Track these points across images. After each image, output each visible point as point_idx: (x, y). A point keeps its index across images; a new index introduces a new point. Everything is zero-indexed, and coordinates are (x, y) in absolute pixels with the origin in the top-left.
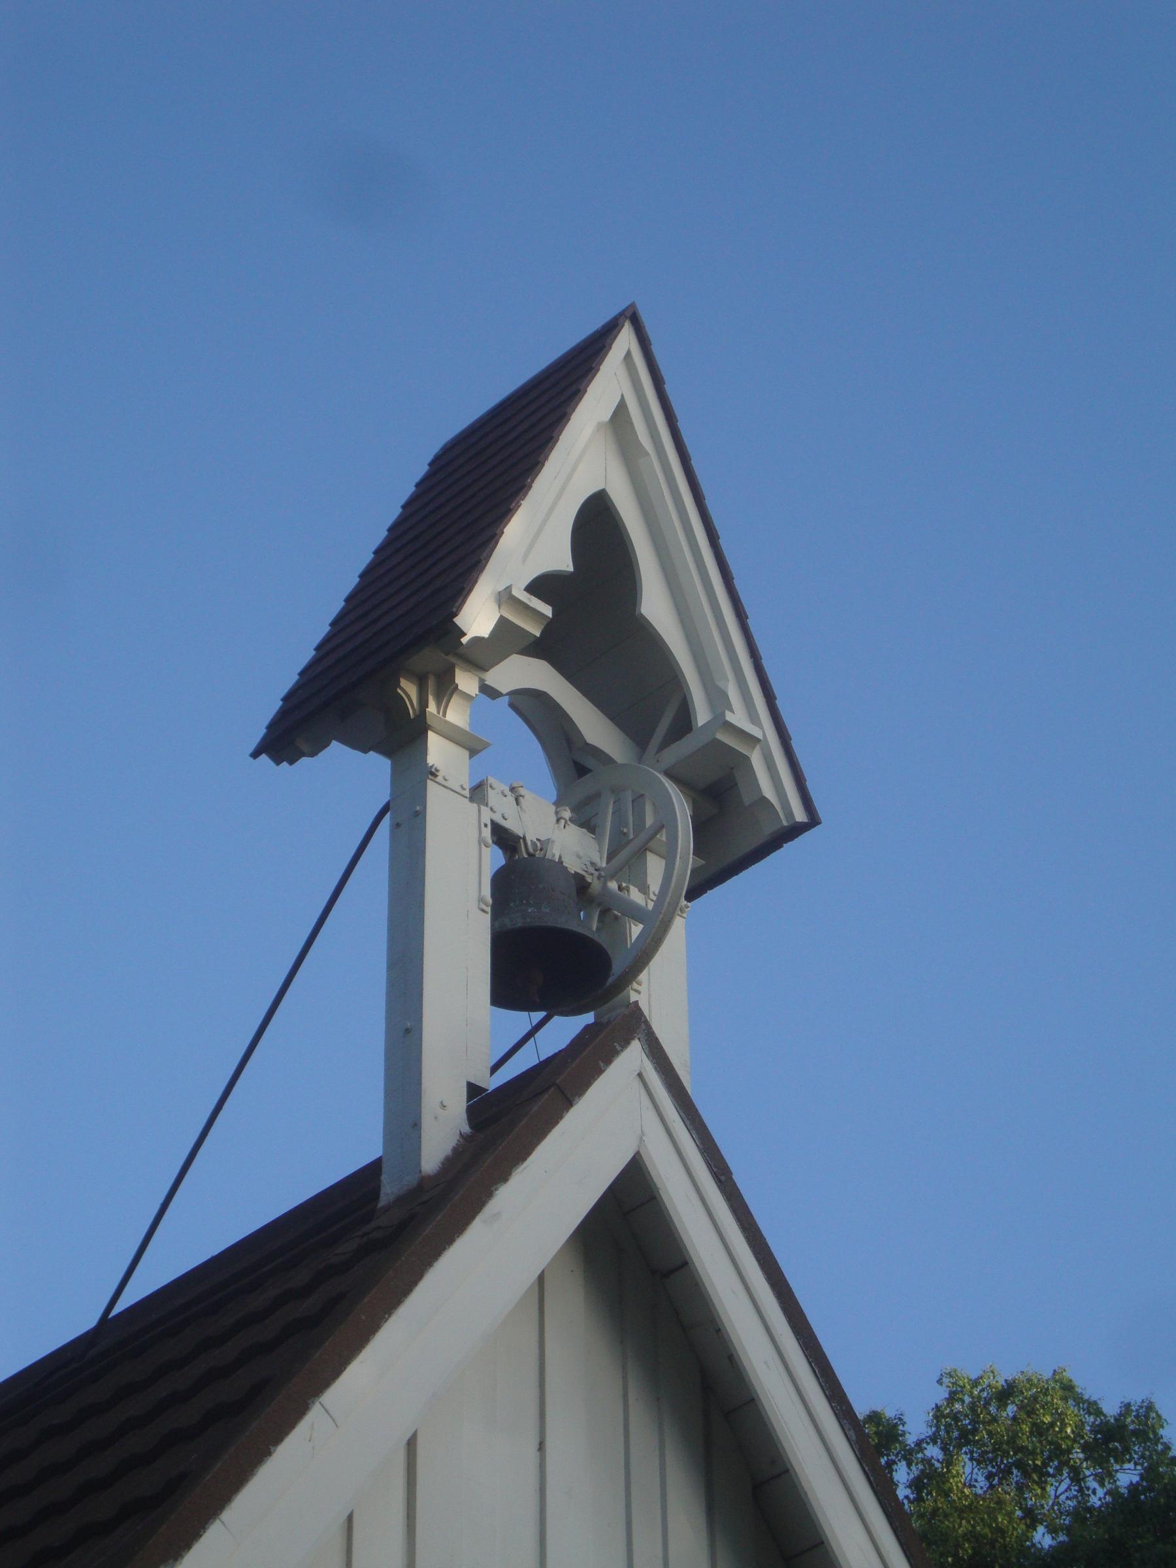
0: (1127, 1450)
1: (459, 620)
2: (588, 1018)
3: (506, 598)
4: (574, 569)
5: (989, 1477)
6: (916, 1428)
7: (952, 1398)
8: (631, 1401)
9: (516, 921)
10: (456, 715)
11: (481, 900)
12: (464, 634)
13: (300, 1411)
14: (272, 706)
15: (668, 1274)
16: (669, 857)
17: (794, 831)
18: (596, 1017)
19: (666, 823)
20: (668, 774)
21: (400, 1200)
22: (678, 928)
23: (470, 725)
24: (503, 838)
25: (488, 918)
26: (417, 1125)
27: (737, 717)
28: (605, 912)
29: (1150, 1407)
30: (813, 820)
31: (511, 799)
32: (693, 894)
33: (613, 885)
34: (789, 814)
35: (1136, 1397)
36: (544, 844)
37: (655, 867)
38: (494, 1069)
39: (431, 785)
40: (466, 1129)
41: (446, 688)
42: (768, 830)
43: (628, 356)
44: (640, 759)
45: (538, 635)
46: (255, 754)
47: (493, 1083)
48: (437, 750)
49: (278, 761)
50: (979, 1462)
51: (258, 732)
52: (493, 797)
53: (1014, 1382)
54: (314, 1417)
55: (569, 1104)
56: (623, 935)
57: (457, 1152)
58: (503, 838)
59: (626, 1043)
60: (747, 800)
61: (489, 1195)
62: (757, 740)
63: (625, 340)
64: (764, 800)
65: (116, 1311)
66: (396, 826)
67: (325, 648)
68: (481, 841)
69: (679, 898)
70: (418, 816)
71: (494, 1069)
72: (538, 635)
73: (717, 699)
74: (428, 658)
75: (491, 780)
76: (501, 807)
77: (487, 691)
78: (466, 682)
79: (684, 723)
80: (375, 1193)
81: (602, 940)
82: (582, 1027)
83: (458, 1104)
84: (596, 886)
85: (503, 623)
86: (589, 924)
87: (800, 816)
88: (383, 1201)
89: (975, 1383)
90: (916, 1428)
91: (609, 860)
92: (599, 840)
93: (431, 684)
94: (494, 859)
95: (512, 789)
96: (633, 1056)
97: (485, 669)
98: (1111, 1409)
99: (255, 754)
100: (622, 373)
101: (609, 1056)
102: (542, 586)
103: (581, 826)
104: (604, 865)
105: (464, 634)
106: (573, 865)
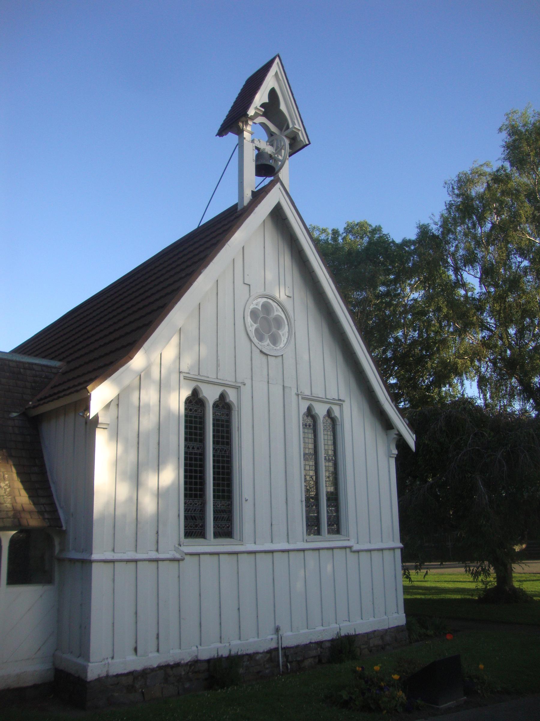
0: (376, 233)
1: (248, 113)
2: (272, 178)
3: (256, 108)
4: (269, 101)
5: (354, 238)
6: (341, 231)
7: (348, 226)
8: (279, 239)
9: (259, 163)
10: (249, 128)
11: (253, 160)
12: (249, 115)
13: (224, 245)
14: (219, 127)
15: (285, 220)
16: (285, 150)
17: (307, 145)
18: (274, 178)
19: (285, 145)
20: (286, 136)
21: (241, 210)
22: (287, 163)
23: (251, 130)
24: (257, 148)
25: (254, 163)
26: (243, 198)
27: (297, 126)
28: (275, 160)
29: (380, 226)
30: (310, 143)
31: (258, 142)
32: (290, 156)
33: (276, 156)
34: (305, 142)
35: (378, 224)
36: (264, 149)
37: (283, 151)
38: (256, 188)
39: (244, 140)
40: (251, 198)
41: (247, 124)
42: (302, 146)
43: (278, 63)
44: (281, 133)
45: (262, 114)
46: (216, 136)
47: (255, 190)
48: (246, 134)
49: (220, 137)
50: (353, 235)
51: (216, 132)
52: (255, 142)
53: (506, 142)
54: (226, 246)
55: (267, 194)
56: (277, 164)
57: (250, 202)
58: (257, 148)
59: (277, 183)
60: (299, 140)
61: (254, 209)
62: (300, 130)
63: (277, 60)
64: (301, 140)
65: (201, 225)
66: (239, 147)
67: (228, 116)
68: (253, 150)
69: (287, 156)
70: (243, 146)
71: (256, 188)
72: (262, 114)
73: (294, 123)
74: (243, 119)
75: (255, 139)
76: (257, 143)
77: (255, 123)
78: (250, 122)
79: (288, 127)
80: (237, 209)
81: (275, 166)
82: (270, 180)
83: (250, 194)
84: (273, 156)
85: (256, 113)
86: (271, 162)
87: (307, 143)
88: (238, 210)
89: (352, 223)
90: (341, 231)
91: (276, 150)
92: (274, 148)
93: (244, 123)
94: (256, 152)
95: (259, 140)
96: (278, 185)
97: (253, 120)
98: (374, 226)
99: (216, 136)
100: (277, 66)
101: (274, 186)
102: (263, 106)
103: (271, 145)
104: (275, 152)
105: (249, 115)
106: (269, 153)
